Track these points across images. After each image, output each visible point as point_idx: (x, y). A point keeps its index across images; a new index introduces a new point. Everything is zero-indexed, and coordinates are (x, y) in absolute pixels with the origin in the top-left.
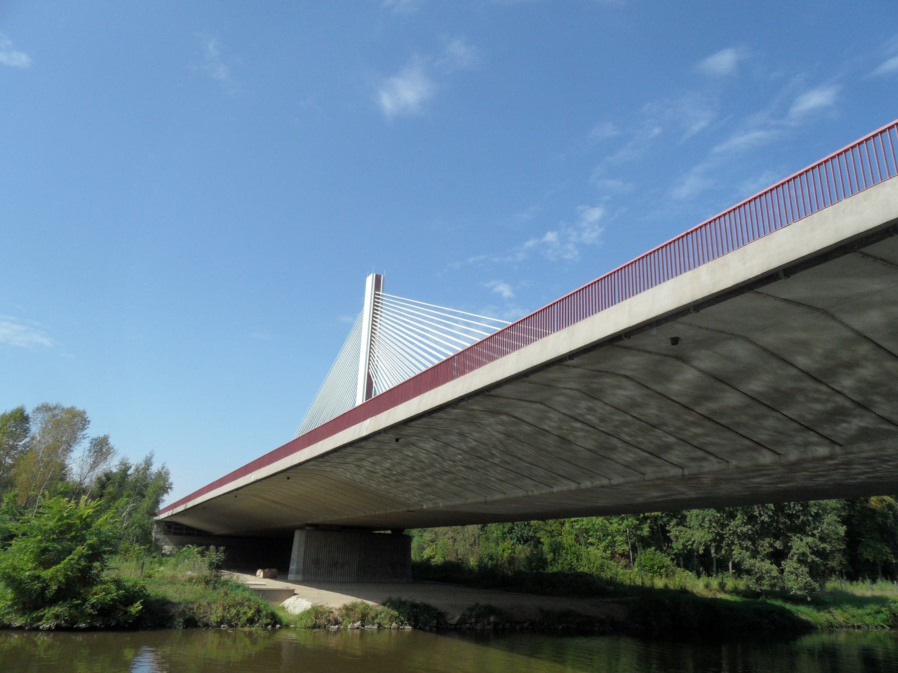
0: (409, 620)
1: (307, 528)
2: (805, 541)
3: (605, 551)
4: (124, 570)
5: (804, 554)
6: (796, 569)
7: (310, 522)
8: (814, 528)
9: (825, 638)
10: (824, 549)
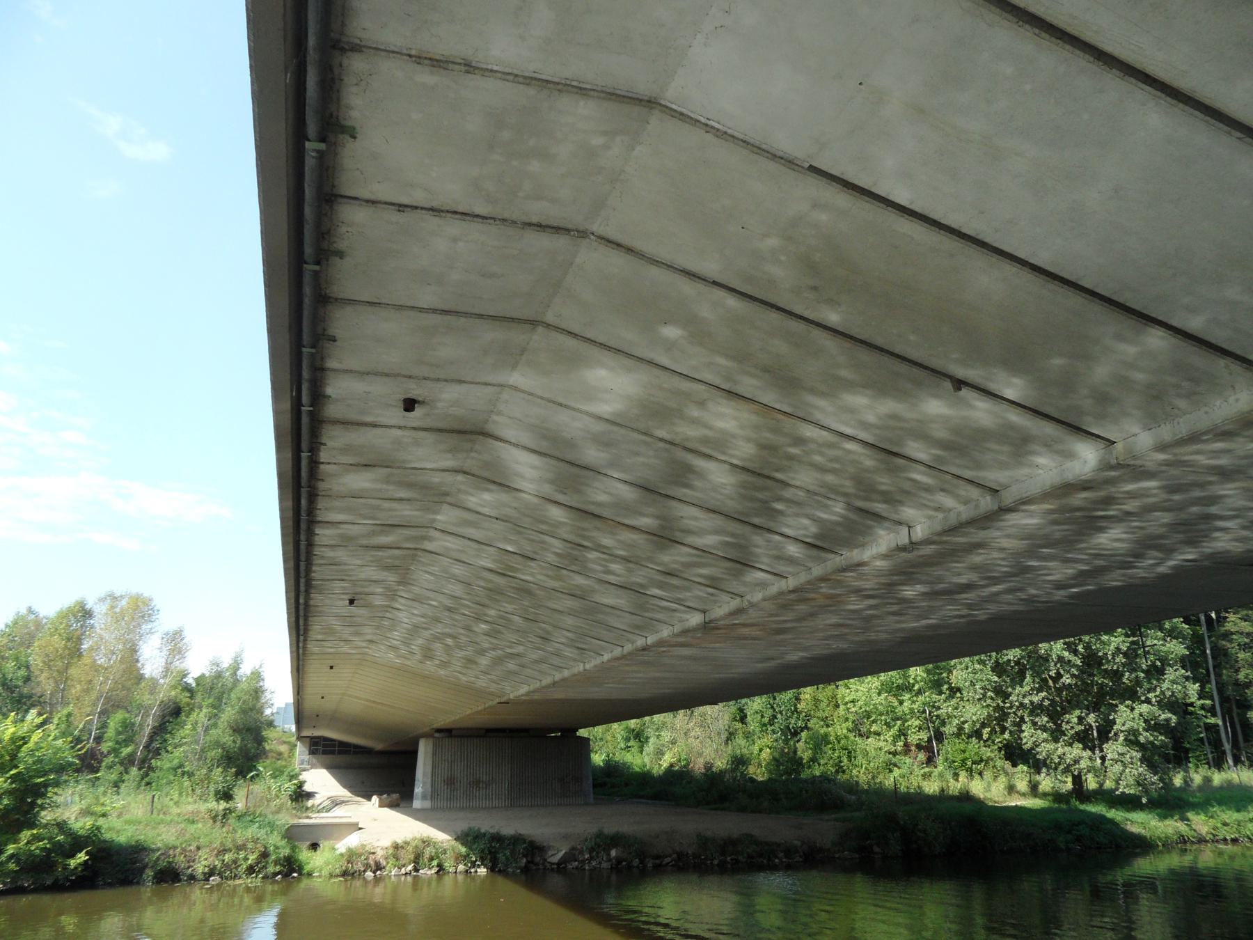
0: (482, 859)
1: (437, 735)
2: (1137, 712)
3: (894, 742)
4: (70, 807)
5: (1135, 732)
6: (1122, 754)
7: (435, 726)
8: (1149, 691)
9: (1172, 861)
10: (1168, 720)
